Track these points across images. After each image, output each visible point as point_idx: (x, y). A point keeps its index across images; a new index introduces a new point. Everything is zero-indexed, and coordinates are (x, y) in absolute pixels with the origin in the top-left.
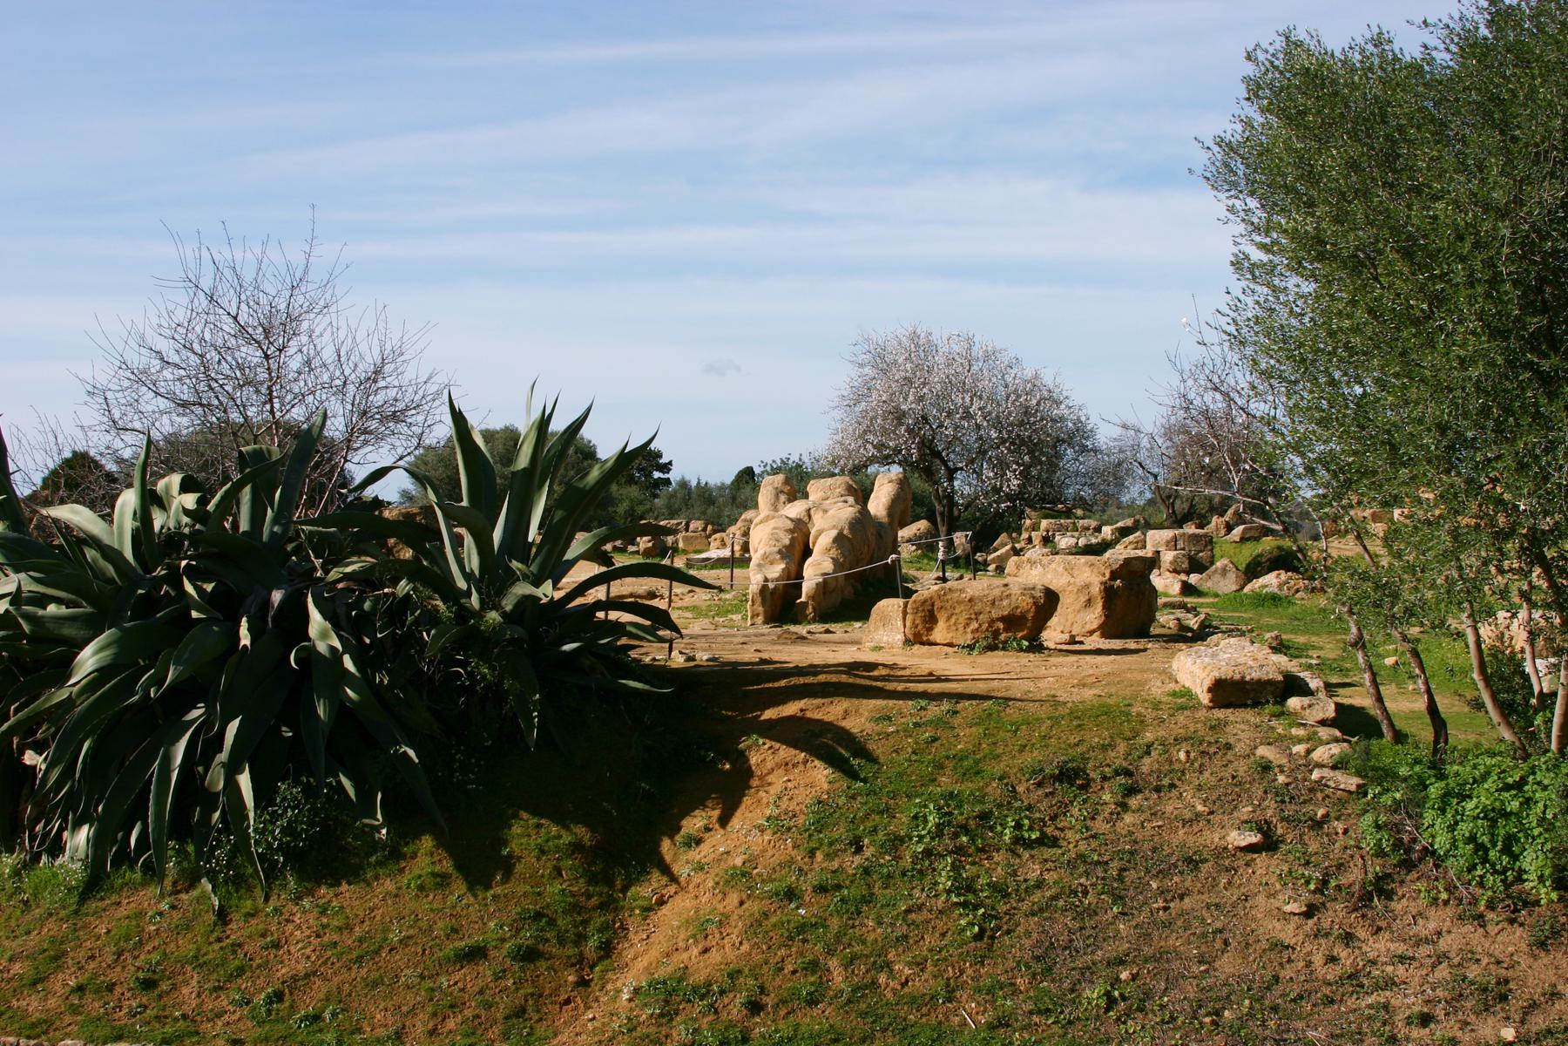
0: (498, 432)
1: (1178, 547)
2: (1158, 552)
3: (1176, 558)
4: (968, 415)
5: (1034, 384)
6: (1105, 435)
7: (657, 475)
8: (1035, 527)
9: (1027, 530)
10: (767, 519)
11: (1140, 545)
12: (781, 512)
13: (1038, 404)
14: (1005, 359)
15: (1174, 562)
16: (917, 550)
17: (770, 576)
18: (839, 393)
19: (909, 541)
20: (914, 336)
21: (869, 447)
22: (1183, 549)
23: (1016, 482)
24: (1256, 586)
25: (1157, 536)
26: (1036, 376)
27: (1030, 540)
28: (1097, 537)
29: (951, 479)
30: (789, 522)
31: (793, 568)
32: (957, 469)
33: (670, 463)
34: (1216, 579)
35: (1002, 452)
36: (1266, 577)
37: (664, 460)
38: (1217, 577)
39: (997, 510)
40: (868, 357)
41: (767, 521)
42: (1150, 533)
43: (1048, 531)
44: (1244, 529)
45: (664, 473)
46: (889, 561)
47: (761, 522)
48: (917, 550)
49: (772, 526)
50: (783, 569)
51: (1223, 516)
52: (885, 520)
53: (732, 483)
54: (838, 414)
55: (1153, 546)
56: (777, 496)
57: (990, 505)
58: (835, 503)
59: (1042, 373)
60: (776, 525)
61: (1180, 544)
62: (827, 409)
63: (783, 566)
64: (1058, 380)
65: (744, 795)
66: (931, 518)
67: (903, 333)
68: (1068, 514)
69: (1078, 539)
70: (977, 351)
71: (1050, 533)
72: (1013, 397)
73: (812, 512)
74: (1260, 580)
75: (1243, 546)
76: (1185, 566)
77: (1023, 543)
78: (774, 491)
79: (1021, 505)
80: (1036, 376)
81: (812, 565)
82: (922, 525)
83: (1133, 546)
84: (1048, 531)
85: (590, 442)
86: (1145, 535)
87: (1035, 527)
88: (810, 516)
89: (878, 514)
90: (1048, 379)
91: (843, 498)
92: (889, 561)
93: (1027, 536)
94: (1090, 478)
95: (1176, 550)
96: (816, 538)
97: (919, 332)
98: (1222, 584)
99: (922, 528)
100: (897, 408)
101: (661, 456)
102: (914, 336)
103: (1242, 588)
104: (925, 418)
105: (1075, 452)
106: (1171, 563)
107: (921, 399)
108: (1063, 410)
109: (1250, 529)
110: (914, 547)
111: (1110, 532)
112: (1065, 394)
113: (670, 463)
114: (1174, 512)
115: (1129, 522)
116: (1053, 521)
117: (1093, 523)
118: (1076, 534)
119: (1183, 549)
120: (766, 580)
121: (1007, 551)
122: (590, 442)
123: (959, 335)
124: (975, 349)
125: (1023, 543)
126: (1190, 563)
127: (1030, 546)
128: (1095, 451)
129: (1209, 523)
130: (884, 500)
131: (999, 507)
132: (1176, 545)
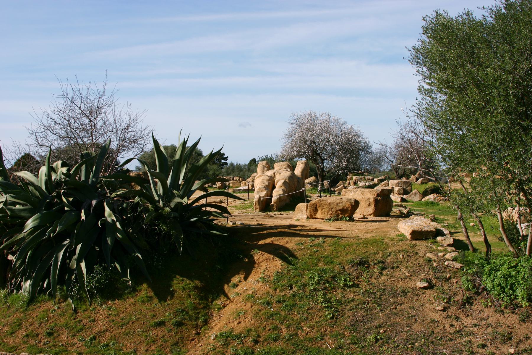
0: (169, 147)
1: (400, 186)
2: (393, 187)
3: (399, 189)
4: (328, 141)
5: (351, 130)
6: (375, 148)
7: (223, 161)
8: (351, 179)
9: (348, 180)
10: (260, 176)
11: (387, 185)
12: (265, 174)
13: (352, 137)
14: (341, 122)
15: (398, 191)
16: (311, 187)
17: (261, 196)
18: (285, 133)
19: (308, 183)
20: (310, 114)
21: (295, 152)
22: (401, 186)
23: (345, 164)
24: (426, 199)
25: (393, 182)
26: (352, 128)
27: (349, 183)
28: (372, 182)
29: (323, 163)
30: (268, 177)
31: (269, 193)
32: (325, 159)
33: (227, 157)
34: (412, 197)
35: (340, 153)
36: (430, 196)
37: (225, 156)
38: (413, 196)
39: (338, 173)
40: (295, 121)
41: (260, 177)
42: (390, 181)
43: (356, 180)
44: (422, 180)
45: (225, 161)
46: (302, 190)
47: (258, 177)
48: (311, 187)
49: (262, 179)
50: (266, 193)
51: (415, 175)
52: (300, 176)
53: (249, 164)
54: (284, 141)
55: (391, 185)
56: (264, 168)
57: (336, 171)
58: (283, 171)
59: (354, 127)
60: (263, 178)
61: (400, 185)
62: (281, 139)
63: (266, 192)
64: (359, 129)
65: (253, 270)
66: (316, 176)
67: (306, 113)
68: (362, 174)
69: (366, 183)
70: (332, 119)
71: (356, 181)
72: (344, 135)
73: (276, 174)
74: (428, 197)
75: (422, 185)
76: (402, 192)
77: (347, 184)
78: (262, 167)
79: (346, 171)
80: (352, 128)
81: (275, 192)
82: (313, 178)
83: (384, 185)
84: (356, 180)
85: (200, 150)
86: (389, 182)
87: (351, 179)
88: (275, 175)
89: (298, 174)
90: (355, 129)
91: (286, 169)
92: (302, 190)
93: (348, 182)
94: (370, 162)
95: (399, 187)
96: (277, 183)
97: (312, 113)
98: (414, 198)
99: (313, 179)
100: (304, 139)
101: (224, 155)
102: (310, 114)
103: (421, 200)
104: (314, 142)
105: (365, 153)
106: (397, 191)
107: (312, 135)
108: (361, 139)
109: (424, 179)
110: (310, 186)
111: (377, 181)
112: (361, 134)
113: (227, 157)
114: (398, 174)
115: (383, 177)
116: (357, 177)
117: (371, 178)
118: (365, 181)
119: (401, 186)
120: (260, 197)
121: (342, 187)
122: (200, 150)
123: (325, 114)
124: (331, 119)
125: (347, 184)
126: (404, 191)
127: (349, 185)
128: (372, 153)
129: (410, 177)
130: (300, 170)
131: (339, 172)
132: (399, 185)
